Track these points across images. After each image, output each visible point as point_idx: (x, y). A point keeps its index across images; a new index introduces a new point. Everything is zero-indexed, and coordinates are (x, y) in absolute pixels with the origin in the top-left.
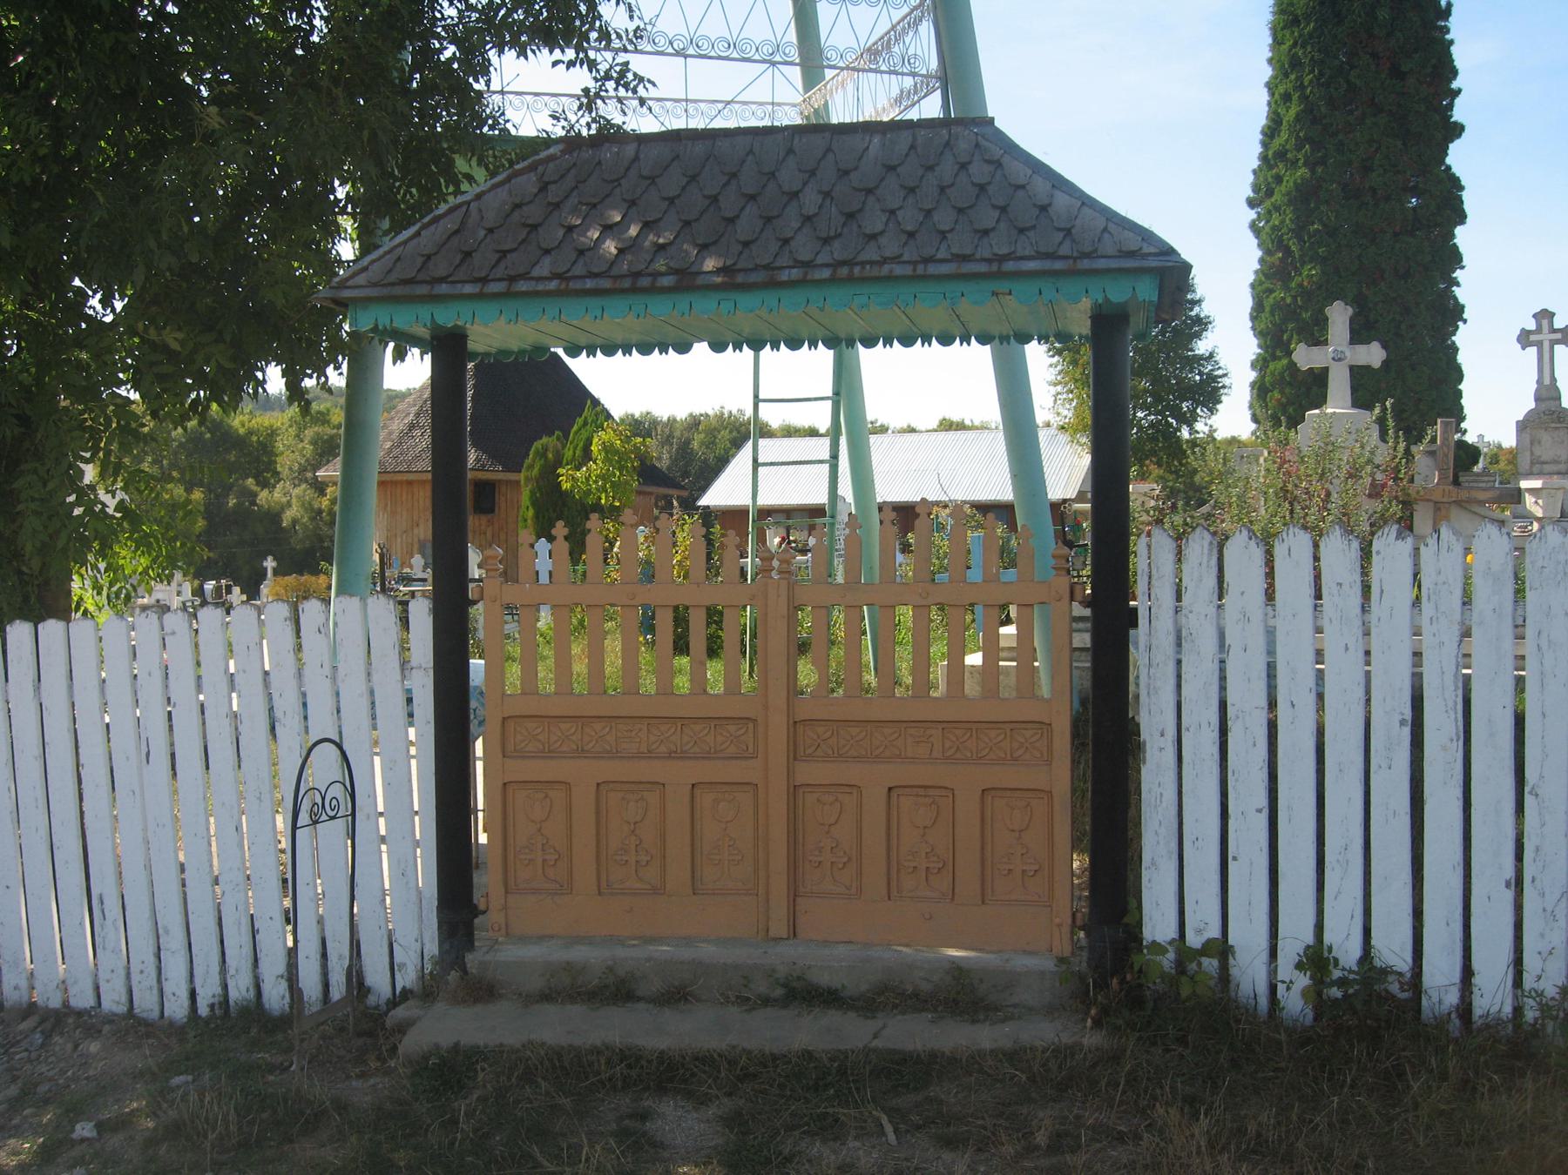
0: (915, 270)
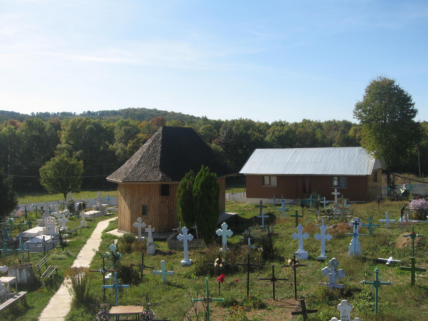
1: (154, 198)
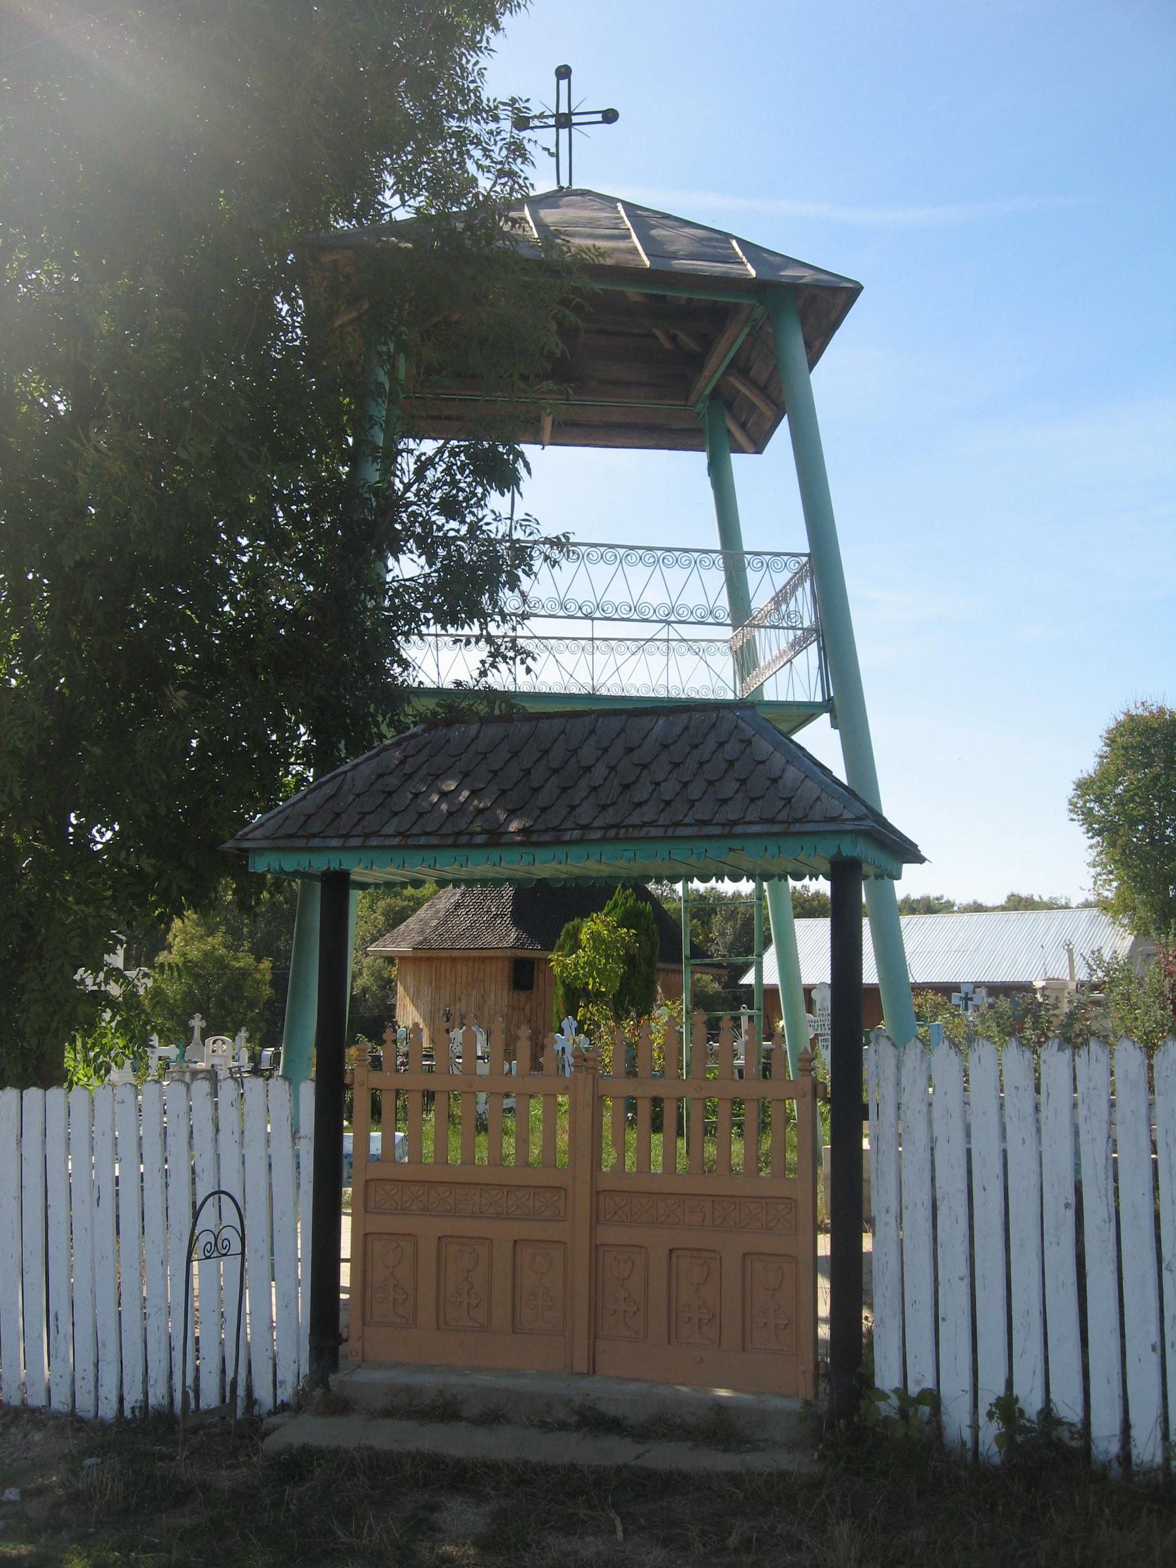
0: (666, 832)
1: (493, 997)
